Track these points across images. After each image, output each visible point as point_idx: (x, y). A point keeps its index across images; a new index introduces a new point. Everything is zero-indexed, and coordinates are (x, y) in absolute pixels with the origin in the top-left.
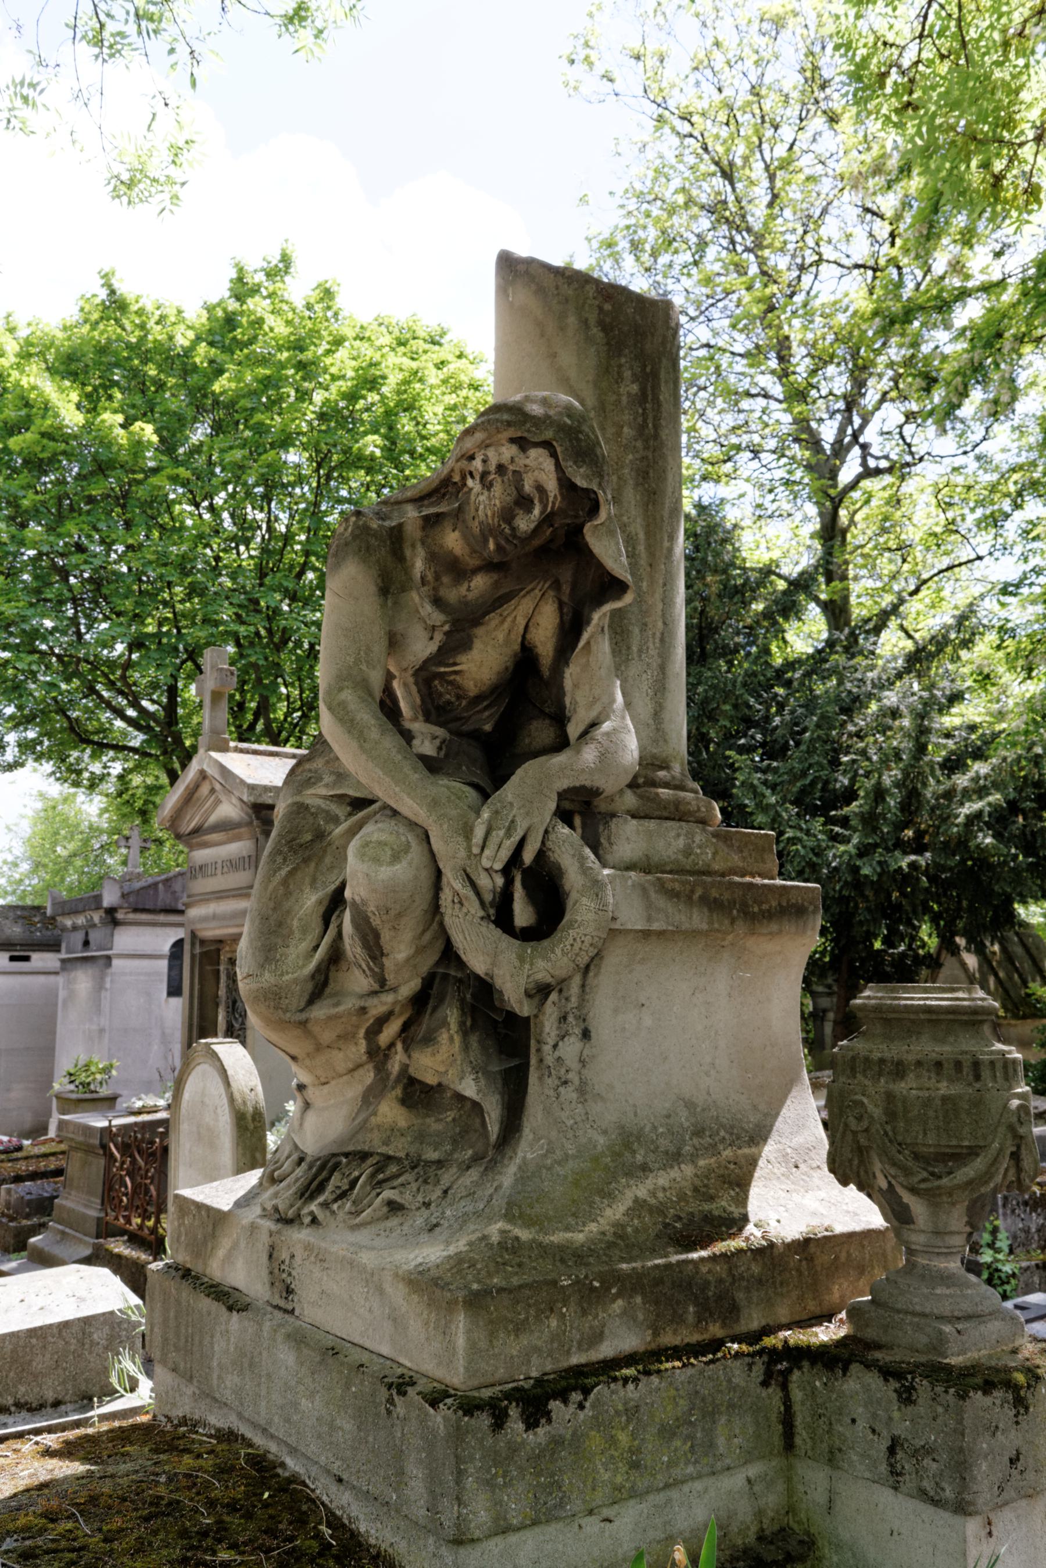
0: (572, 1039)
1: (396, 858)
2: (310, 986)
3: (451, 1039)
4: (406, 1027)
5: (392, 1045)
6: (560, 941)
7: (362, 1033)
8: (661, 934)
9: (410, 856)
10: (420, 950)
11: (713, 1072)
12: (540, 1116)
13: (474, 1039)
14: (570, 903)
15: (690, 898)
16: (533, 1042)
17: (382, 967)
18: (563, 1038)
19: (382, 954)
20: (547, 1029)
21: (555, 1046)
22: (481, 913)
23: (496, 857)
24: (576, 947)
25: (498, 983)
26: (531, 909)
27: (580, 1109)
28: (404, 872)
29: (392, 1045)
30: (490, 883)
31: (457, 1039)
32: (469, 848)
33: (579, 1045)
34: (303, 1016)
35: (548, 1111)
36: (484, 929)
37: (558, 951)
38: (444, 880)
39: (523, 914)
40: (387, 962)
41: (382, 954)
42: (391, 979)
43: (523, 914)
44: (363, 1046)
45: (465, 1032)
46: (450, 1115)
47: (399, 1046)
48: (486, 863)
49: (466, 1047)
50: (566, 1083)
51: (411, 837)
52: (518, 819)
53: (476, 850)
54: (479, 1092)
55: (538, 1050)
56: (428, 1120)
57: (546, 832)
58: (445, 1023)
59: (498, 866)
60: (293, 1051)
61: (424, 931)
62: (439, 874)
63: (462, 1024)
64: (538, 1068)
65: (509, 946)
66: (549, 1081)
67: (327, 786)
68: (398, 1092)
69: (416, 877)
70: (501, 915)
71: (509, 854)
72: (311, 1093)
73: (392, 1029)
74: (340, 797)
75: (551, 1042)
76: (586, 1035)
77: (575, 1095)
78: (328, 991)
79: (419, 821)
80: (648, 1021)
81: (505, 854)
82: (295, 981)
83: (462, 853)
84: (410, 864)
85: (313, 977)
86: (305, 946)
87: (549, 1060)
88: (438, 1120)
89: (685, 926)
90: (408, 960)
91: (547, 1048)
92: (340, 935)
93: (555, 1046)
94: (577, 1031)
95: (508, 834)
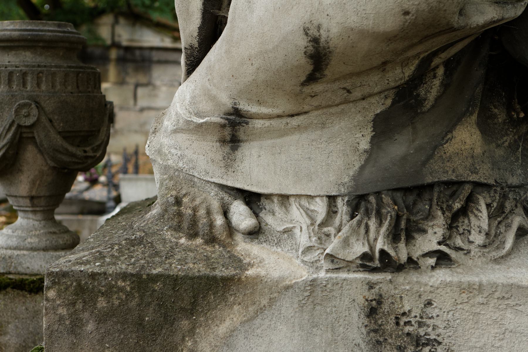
5: (437, 67)
88: (498, 146)
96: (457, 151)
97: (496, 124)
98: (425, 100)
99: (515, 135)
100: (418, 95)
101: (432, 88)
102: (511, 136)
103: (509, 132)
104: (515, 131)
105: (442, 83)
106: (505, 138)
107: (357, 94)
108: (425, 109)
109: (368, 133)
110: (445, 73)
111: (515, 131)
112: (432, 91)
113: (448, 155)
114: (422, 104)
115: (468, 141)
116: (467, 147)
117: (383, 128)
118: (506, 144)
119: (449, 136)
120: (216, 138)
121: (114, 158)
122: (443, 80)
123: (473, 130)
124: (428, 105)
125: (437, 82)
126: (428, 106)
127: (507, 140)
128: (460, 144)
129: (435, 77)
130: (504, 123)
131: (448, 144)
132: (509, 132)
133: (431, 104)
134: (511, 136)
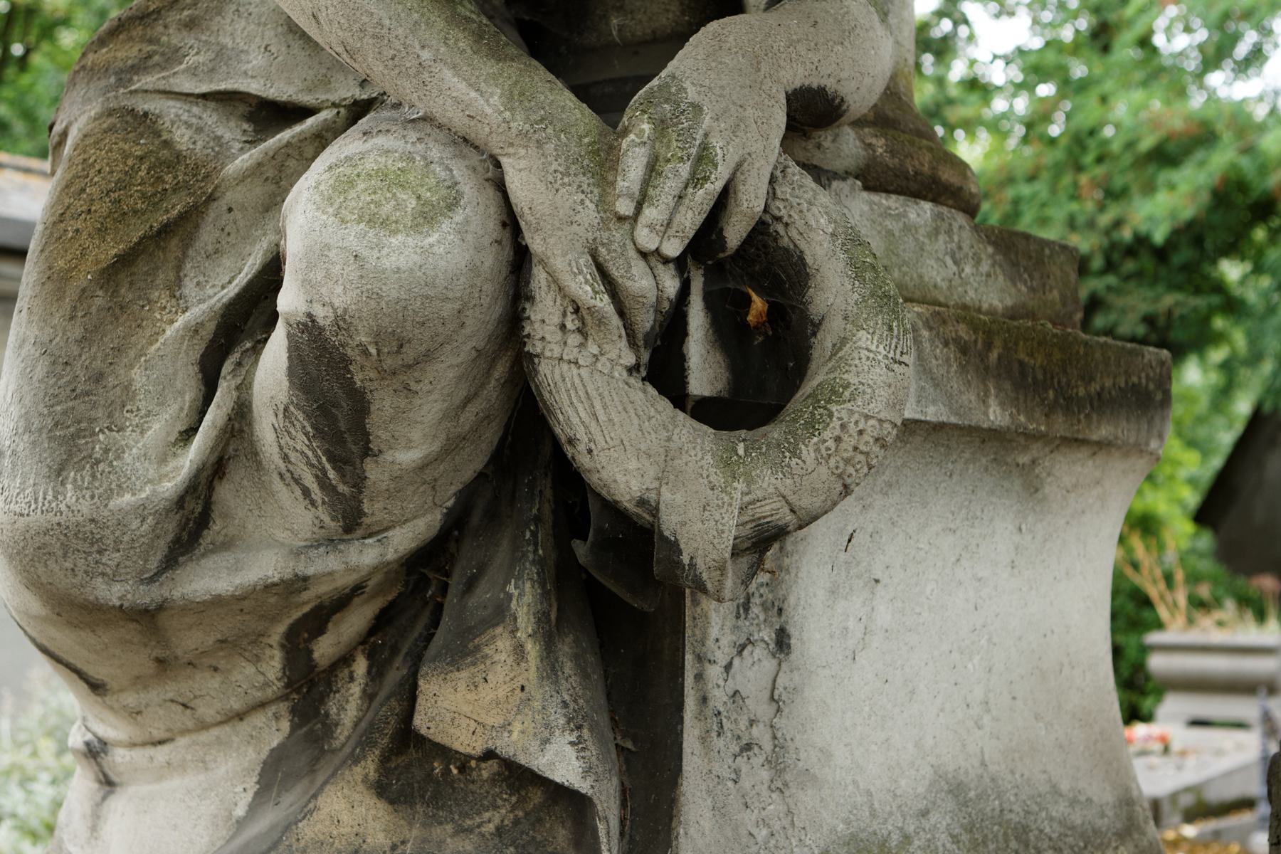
0: (759, 652)
1: (427, 217)
2: (171, 527)
3: (519, 651)
4: (382, 621)
5: (345, 660)
6: (812, 427)
7: (281, 629)
8: (939, 427)
9: (459, 216)
10: (451, 448)
11: (986, 720)
12: (707, 824)
13: (565, 648)
14: (824, 342)
15: (983, 357)
16: (689, 658)
17: (359, 482)
18: (741, 649)
19: (367, 452)
20: (714, 632)
21: (728, 667)
22: (630, 359)
23: (669, 223)
24: (849, 442)
25: (670, 523)
26: (719, 357)
27: (775, 807)
28: (441, 253)
29: (345, 660)
30: (649, 286)
31: (533, 650)
32: (603, 204)
33: (769, 665)
34: (147, 596)
35: (719, 810)
36: (638, 396)
37: (808, 453)
38: (539, 277)
39: (704, 370)
40: (374, 472)
41: (367, 452)
42: (374, 509)
43: (704, 370)
44: (273, 665)
45: (548, 635)
46: (491, 820)
47: (360, 666)
48: (647, 239)
49: (551, 670)
50: (748, 747)
51: (460, 171)
52: (717, 142)
53: (625, 207)
54: (587, 771)
55: (699, 677)
56: (437, 831)
57: (773, 180)
58: (500, 613)
59: (673, 248)
60: (98, 671)
61: (467, 401)
62: (520, 260)
63: (542, 619)
64: (700, 716)
65: (696, 443)
66: (719, 743)
67: (193, 72)
68: (370, 766)
69: (474, 269)
70: (662, 368)
71: (699, 220)
72: (120, 758)
73: (355, 621)
74: (225, 99)
75: (722, 659)
76: (782, 642)
77: (765, 774)
78: (208, 537)
79: (480, 133)
80: (884, 616)
81: (690, 220)
82: (140, 510)
83: (589, 214)
84: (461, 232)
85: (180, 502)
86: (161, 426)
87: (719, 698)
88: (461, 831)
89: (976, 419)
90: (423, 467)
91: (714, 672)
92: (241, 414)
93: (728, 667)
94: (767, 634)
95: (696, 180)
96: (322, 837)
97: (473, 782)
98: (337, 725)
99: (513, 808)
100: (327, 715)
101: (347, 701)
102: (503, 811)
103: (500, 802)
104: (514, 799)
105: (364, 691)
106: (487, 815)
107: (207, 711)
108: (336, 744)
109: (252, 785)
110: (369, 672)
111: (514, 799)
112: (348, 707)
113: (302, 843)
114: (333, 732)
115: (345, 817)
116: (342, 830)
117: (274, 775)
118: (491, 827)
119: (311, 806)
120: (110, 758)
121: (998, 271)
122: (367, 685)
123: (357, 796)
124: (343, 733)
125: (356, 689)
126: (342, 739)
127: (491, 820)
128: (327, 823)
129: (352, 679)
130: (493, 780)
131: (305, 822)
132: (500, 802)
133: (346, 733)
134: (503, 811)
